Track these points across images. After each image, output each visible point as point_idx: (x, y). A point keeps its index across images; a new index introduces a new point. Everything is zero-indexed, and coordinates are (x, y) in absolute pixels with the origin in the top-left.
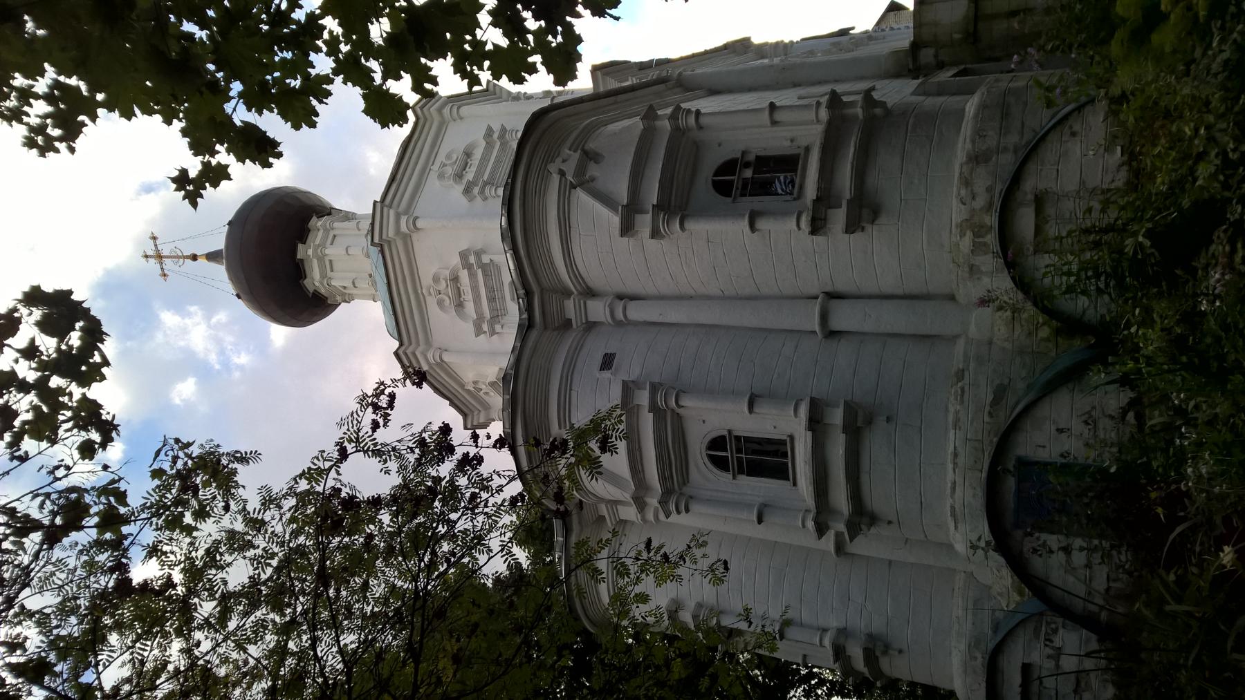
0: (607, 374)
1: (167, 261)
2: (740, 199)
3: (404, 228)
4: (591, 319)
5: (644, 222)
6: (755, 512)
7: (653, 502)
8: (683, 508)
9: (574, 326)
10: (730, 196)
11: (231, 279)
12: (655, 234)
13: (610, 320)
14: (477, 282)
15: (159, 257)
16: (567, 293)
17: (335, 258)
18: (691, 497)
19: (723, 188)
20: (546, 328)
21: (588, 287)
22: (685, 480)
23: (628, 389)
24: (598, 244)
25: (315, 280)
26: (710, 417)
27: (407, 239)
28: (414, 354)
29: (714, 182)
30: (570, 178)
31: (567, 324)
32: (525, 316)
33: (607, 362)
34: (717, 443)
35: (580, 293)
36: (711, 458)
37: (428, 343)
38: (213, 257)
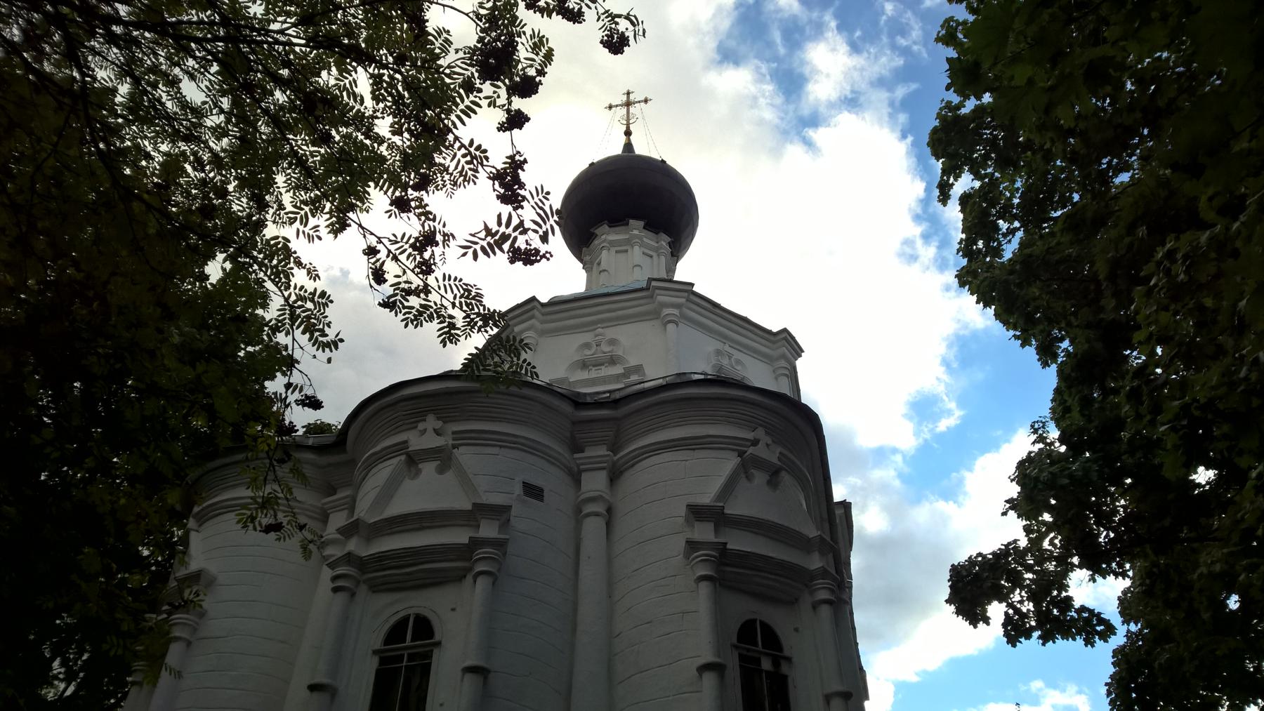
0: (518, 490)
1: (624, 110)
2: (736, 654)
3: (666, 311)
4: (585, 476)
5: (704, 532)
6: (325, 680)
7: (354, 546)
8: (340, 583)
9: (576, 456)
10: (739, 641)
11: (608, 158)
12: (692, 546)
13: (582, 497)
14: (610, 383)
15: (628, 104)
16: (614, 449)
17: (630, 256)
18: (353, 595)
19: (747, 631)
20: (574, 423)
21: (622, 473)
22: (377, 588)
23: (500, 512)
24: (677, 480)
25: (607, 235)
26: (459, 619)
27: (655, 315)
28: (532, 317)
29: (754, 621)
30: (751, 450)
31: (577, 448)
32: (589, 400)
33: (532, 491)
34: (424, 627)
35: (614, 464)
36: (405, 620)
37: (543, 333)
38: (628, 147)
